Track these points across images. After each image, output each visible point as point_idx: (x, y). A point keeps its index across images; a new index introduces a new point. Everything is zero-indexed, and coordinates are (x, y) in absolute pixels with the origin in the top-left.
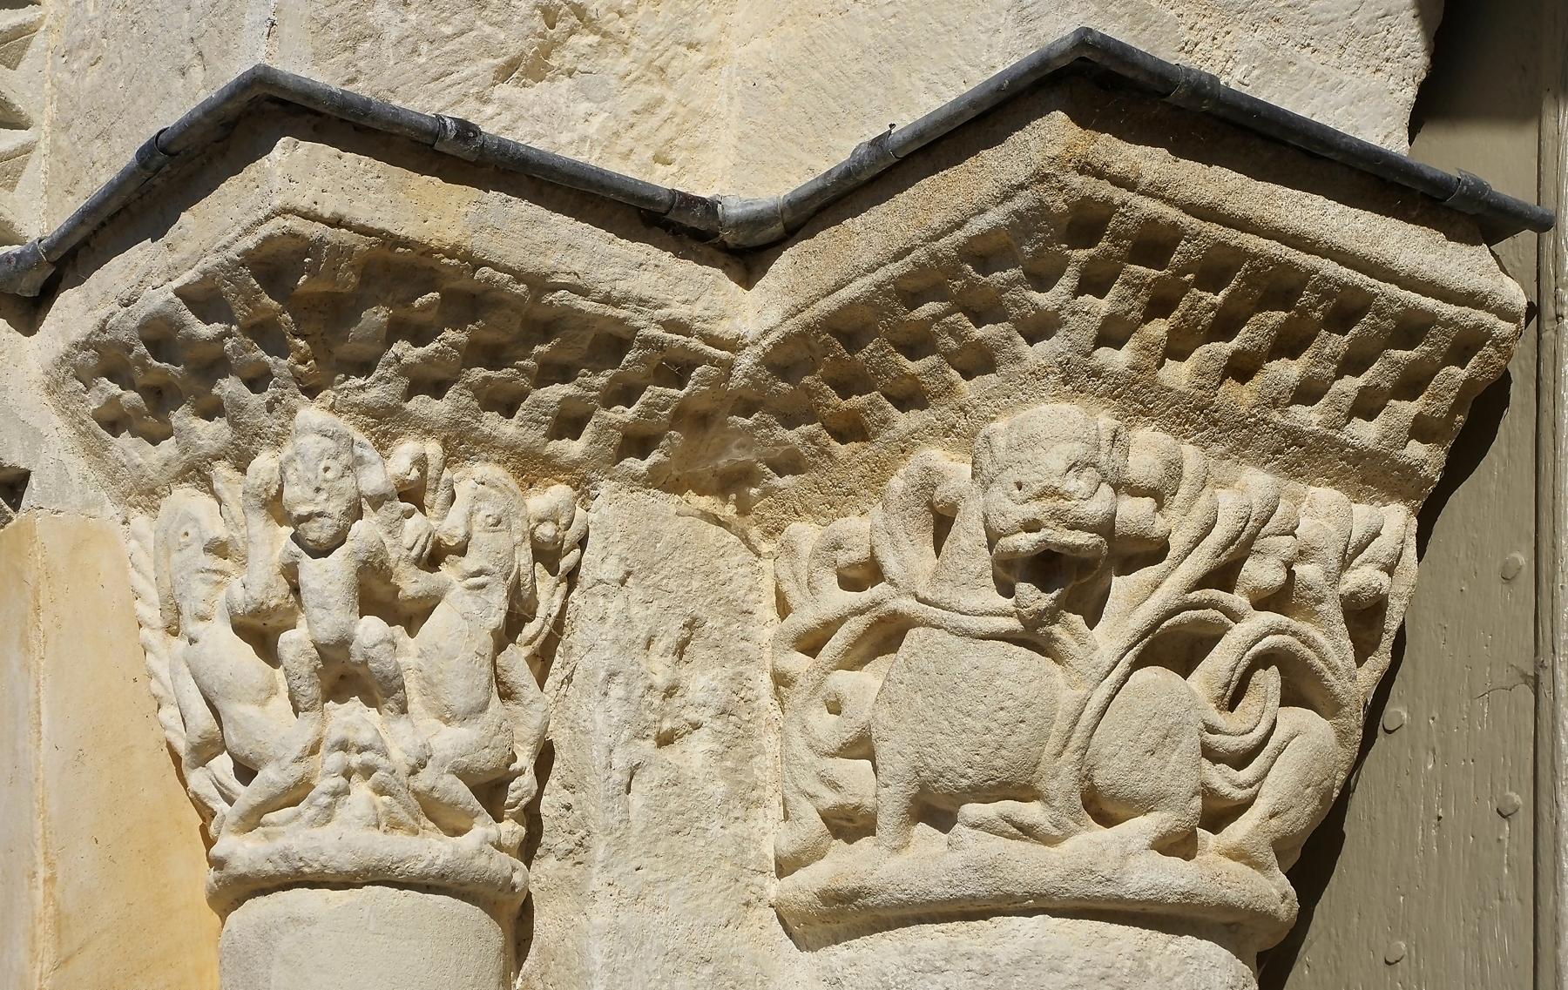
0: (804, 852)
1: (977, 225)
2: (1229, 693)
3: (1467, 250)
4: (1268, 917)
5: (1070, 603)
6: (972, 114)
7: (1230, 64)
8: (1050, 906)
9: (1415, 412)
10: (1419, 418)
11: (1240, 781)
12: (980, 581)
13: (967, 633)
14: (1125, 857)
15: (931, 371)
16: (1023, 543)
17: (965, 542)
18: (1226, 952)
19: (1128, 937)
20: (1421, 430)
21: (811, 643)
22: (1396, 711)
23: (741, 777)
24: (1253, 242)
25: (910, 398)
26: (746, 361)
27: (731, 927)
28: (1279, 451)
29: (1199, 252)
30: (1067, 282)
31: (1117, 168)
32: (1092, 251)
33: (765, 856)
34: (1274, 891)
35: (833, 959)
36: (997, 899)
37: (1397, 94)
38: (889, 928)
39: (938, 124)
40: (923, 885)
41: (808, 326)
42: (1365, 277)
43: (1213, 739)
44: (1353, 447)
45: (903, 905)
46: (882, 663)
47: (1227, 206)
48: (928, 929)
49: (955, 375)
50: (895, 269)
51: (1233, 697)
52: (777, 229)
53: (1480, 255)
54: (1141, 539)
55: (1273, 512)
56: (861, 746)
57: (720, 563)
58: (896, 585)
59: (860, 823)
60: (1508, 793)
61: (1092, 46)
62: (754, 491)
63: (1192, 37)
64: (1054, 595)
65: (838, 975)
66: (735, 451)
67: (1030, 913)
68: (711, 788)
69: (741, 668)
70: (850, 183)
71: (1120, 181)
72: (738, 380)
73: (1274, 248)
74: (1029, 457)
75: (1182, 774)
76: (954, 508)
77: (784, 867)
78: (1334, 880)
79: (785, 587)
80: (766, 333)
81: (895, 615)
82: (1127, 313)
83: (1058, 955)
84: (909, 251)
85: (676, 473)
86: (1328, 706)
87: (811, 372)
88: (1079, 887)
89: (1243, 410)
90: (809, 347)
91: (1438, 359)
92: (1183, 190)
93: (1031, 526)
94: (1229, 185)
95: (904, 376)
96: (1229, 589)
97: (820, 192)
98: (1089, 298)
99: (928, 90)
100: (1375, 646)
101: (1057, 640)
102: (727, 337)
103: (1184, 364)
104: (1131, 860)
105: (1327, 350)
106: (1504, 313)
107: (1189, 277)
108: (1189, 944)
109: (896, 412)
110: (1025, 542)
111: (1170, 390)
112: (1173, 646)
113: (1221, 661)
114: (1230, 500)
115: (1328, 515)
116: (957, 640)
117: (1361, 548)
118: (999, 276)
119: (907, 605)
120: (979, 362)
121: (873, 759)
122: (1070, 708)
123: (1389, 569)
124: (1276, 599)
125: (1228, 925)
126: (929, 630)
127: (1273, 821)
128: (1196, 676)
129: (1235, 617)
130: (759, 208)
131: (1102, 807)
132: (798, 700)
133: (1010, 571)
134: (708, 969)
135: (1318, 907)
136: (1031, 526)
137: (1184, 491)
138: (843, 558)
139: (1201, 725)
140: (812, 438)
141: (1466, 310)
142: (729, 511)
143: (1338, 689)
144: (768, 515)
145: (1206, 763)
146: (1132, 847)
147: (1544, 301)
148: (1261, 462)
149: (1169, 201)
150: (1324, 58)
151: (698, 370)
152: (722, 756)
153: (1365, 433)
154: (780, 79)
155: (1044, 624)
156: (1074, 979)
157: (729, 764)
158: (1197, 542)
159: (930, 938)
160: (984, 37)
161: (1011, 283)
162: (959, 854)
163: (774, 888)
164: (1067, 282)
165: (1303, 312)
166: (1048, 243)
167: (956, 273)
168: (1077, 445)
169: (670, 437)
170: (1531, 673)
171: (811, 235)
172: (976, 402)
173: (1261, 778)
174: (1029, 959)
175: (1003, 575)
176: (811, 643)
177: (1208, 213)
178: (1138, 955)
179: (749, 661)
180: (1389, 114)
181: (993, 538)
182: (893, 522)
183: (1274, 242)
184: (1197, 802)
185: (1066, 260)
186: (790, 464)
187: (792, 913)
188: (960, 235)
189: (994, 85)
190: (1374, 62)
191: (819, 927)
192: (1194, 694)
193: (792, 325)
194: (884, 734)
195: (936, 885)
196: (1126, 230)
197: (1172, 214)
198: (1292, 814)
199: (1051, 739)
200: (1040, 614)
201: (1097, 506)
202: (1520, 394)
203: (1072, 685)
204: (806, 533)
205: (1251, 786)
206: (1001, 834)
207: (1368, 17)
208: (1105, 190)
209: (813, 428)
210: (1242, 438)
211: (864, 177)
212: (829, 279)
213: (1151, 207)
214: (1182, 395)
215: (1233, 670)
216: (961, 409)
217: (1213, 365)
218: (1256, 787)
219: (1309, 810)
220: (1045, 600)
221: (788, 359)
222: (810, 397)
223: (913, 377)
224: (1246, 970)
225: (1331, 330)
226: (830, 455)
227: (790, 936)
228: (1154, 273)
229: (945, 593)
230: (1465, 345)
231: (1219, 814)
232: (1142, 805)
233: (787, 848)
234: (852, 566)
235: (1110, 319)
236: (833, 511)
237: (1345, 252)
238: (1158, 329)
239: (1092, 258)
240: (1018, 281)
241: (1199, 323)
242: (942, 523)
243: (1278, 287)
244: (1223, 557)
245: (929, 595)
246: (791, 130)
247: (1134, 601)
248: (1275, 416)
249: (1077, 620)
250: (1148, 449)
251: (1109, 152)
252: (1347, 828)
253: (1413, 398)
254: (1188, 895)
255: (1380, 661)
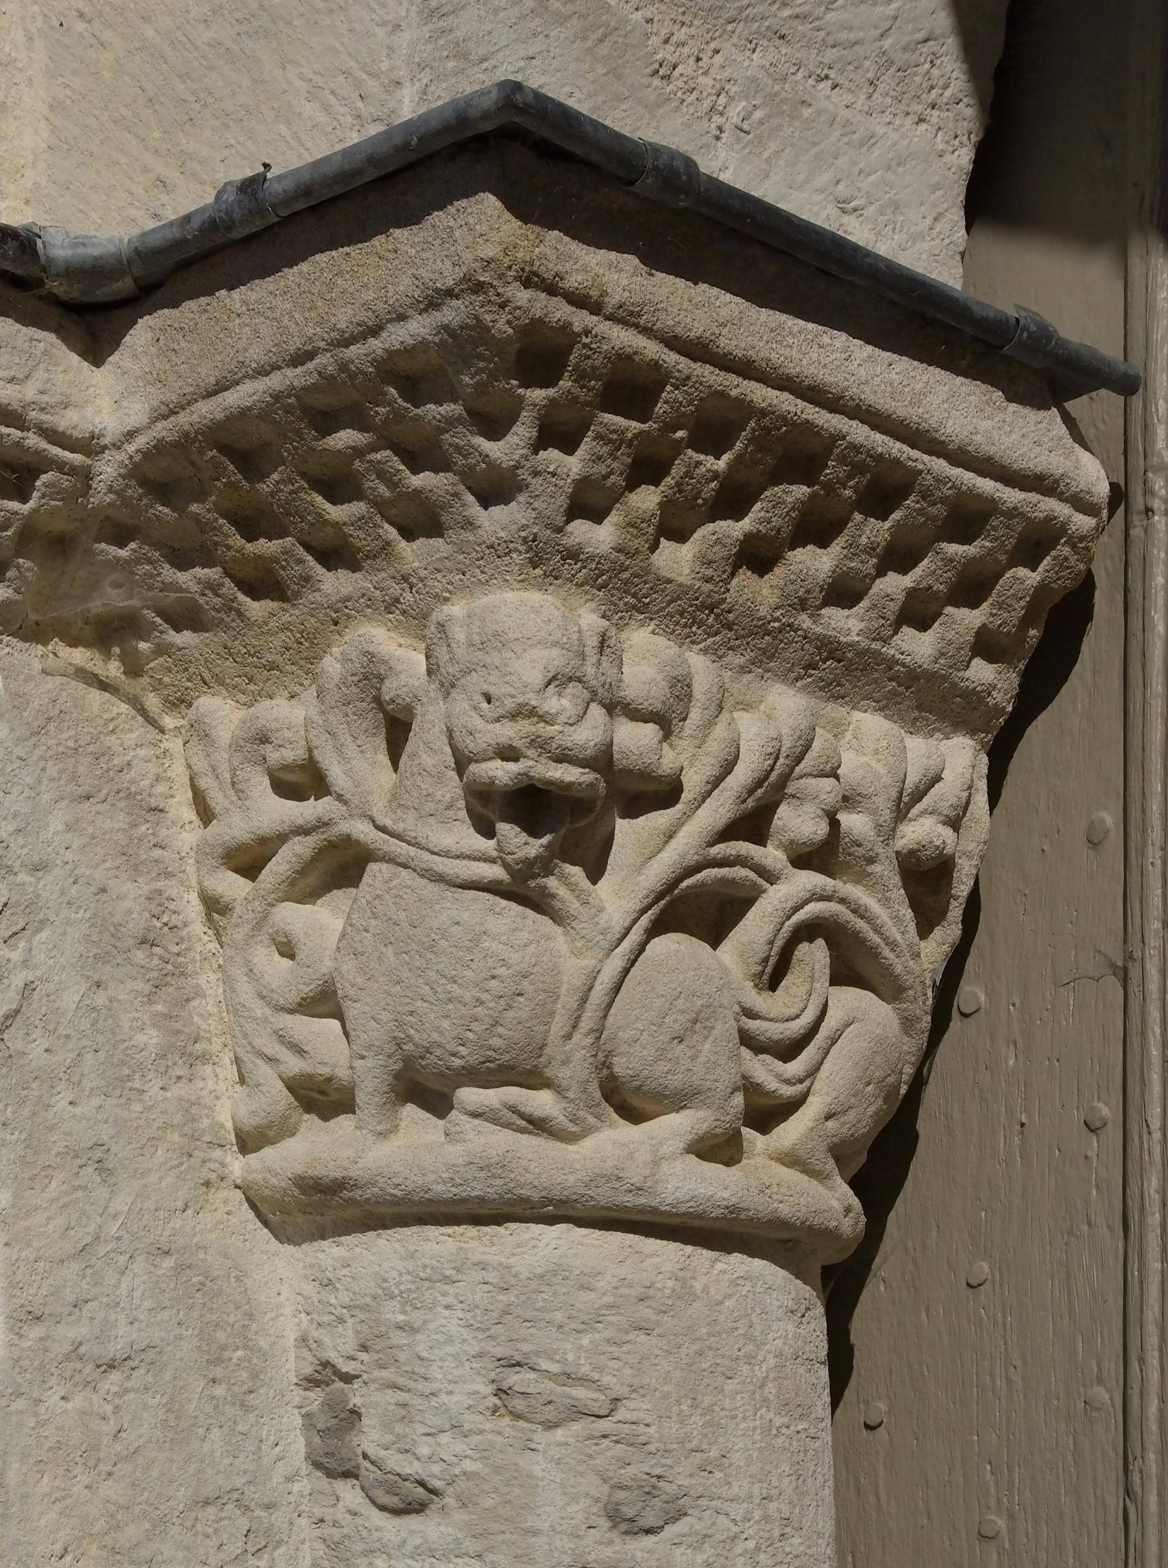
0: (270, 1127)
1: (398, 336)
2: (769, 970)
3: (1032, 415)
4: (828, 1235)
5: (566, 852)
6: (372, 174)
7: (722, 100)
8: (571, 1213)
9: (977, 623)
10: (982, 632)
11: (788, 1075)
12: (450, 813)
13: (439, 878)
14: (656, 1162)
15: (361, 521)
16: (499, 773)
17: (428, 761)
18: (782, 1273)
19: (665, 1256)
20: (986, 645)
21: (249, 861)
22: (971, 991)
23: (178, 1026)
24: (761, 394)
25: (336, 554)
26: (107, 470)
27: (190, 1212)
28: (812, 666)
29: (690, 403)
30: (522, 432)
31: (573, 281)
32: (552, 392)
33: (222, 1126)
34: (835, 1203)
35: (321, 1256)
36: (510, 1203)
37: (948, 158)
38: (385, 1227)
39: (329, 181)
40: (420, 1181)
41: (186, 434)
42: (905, 448)
43: (753, 1025)
44: (903, 665)
45: (397, 1201)
46: (341, 898)
47: (722, 342)
48: (432, 1231)
49: (391, 533)
50: (294, 377)
51: (774, 974)
52: (125, 286)
53: (1050, 422)
54: (645, 775)
55: (807, 747)
56: (324, 1002)
57: (111, 741)
58: (345, 803)
59: (335, 1097)
60: (1096, 1104)
61: (524, 110)
62: (143, 646)
63: (666, 54)
64: (545, 840)
65: (330, 1275)
66: (111, 592)
67: (551, 1220)
68: (140, 1038)
69: (159, 885)
70: (219, 239)
71: (578, 300)
72: (100, 495)
73: (786, 402)
74: (497, 661)
75: (715, 1062)
76: (409, 709)
77: (249, 1141)
78: (908, 1184)
79: (204, 783)
80: (130, 435)
81: (347, 841)
82: (606, 477)
83: (587, 1271)
84: (310, 355)
85: (34, 617)
86: (888, 987)
87: (201, 498)
88: (604, 1195)
89: (763, 611)
90: (192, 463)
91: (1003, 558)
92: (663, 316)
93: (508, 753)
94: (724, 312)
95: (323, 521)
96: (760, 838)
97: (179, 244)
98: (553, 454)
99: (312, 97)
100: (942, 914)
101: (553, 896)
102: (76, 434)
103: (688, 546)
104: (665, 1166)
105: (864, 540)
106: (1081, 503)
107: (680, 434)
108: (738, 1263)
109: (320, 570)
110: (502, 772)
111: (669, 581)
112: (699, 909)
113: (755, 930)
114: (754, 730)
115: (876, 751)
116: (430, 885)
117: (919, 795)
118: (432, 411)
119: (362, 830)
120: (423, 521)
121: (339, 1015)
122: (578, 981)
123: (954, 823)
124: (819, 856)
125: (785, 1242)
126: (393, 868)
127: (830, 1124)
128: (727, 945)
129: (771, 877)
130: (96, 252)
131: (627, 1101)
132: (239, 935)
133: (489, 807)
134: (168, 1263)
135: (892, 1215)
136: (508, 753)
137: (695, 716)
138: (275, 757)
139: (737, 1008)
140: (212, 587)
141: (1033, 497)
142: (113, 670)
143: (899, 969)
144: (166, 680)
145: (746, 1053)
146: (664, 1150)
147: (1132, 486)
148: (790, 677)
149: (647, 331)
150: (848, 98)
151: (44, 478)
152: (150, 999)
153: (918, 646)
154: (97, 24)
155: (535, 876)
156: (608, 1299)
157: (159, 1008)
158: (716, 782)
159: (437, 1243)
160: (380, 33)
161: (451, 422)
162: (457, 1148)
163: (238, 1166)
164: (522, 432)
165: (829, 488)
166: (493, 377)
167: (378, 398)
168: (555, 652)
169: (18, 567)
170: (1120, 964)
171: (175, 304)
172: (423, 573)
173: (813, 1072)
174: (555, 1273)
175: (479, 809)
176: (249, 861)
177: (698, 350)
178: (681, 1274)
179: (168, 875)
180: (936, 187)
181: (462, 763)
182: (331, 717)
183: (786, 395)
184: (739, 1099)
185: (520, 401)
186: (187, 617)
187: (264, 1199)
188: (376, 345)
189: (398, 140)
190: (919, 108)
191: (300, 1218)
192: (725, 970)
193: (162, 430)
194: (352, 992)
195: (436, 1182)
196: (593, 368)
197: (651, 349)
198: (851, 1116)
199: (557, 1018)
200: (529, 863)
201: (588, 734)
202: (1105, 605)
203: (577, 954)
204: (222, 712)
205: (801, 1081)
206: (507, 1125)
207: (905, 40)
208: (560, 311)
209: (212, 573)
210: (766, 646)
211: (236, 235)
212: (208, 375)
213: (622, 338)
214: (684, 589)
215: (771, 943)
216: (405, 578)
217: (720, 552)
218: (807, 1083)
219: (871, 1110)
220: (534, 847)
221: (166, 473)
222: (203, 531)
223: (336, 525)
224: (808, 1291)
225: (868, 513)
226: (240, 614)
227: (266, 1223)
228: (635, 426)
229: (408, 823)
230: (1035, 542)
231: (766, 1113)
232: (677, 1101)
233: (249, 1122)
234: (285, 768)
235: (583, 484)
236: (252, 687)
237: (878, 414)
238: (647, 499)
239: (552, 401)
240: (459, 420)
241: (697, 496)
242: (397, 730)
243: (798, 454)
244: (750, 803)
245: (388, 822)
246: (124, 111)
247: (646, 853)
248: (804, 621)
249: (576, 872)
250: (647, 657)
251: (562, 257)
252: (921, 1126)
253: (974, 604)
254: (734, 1209)
255: (948, 933)
